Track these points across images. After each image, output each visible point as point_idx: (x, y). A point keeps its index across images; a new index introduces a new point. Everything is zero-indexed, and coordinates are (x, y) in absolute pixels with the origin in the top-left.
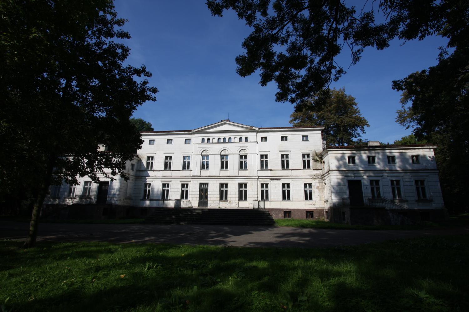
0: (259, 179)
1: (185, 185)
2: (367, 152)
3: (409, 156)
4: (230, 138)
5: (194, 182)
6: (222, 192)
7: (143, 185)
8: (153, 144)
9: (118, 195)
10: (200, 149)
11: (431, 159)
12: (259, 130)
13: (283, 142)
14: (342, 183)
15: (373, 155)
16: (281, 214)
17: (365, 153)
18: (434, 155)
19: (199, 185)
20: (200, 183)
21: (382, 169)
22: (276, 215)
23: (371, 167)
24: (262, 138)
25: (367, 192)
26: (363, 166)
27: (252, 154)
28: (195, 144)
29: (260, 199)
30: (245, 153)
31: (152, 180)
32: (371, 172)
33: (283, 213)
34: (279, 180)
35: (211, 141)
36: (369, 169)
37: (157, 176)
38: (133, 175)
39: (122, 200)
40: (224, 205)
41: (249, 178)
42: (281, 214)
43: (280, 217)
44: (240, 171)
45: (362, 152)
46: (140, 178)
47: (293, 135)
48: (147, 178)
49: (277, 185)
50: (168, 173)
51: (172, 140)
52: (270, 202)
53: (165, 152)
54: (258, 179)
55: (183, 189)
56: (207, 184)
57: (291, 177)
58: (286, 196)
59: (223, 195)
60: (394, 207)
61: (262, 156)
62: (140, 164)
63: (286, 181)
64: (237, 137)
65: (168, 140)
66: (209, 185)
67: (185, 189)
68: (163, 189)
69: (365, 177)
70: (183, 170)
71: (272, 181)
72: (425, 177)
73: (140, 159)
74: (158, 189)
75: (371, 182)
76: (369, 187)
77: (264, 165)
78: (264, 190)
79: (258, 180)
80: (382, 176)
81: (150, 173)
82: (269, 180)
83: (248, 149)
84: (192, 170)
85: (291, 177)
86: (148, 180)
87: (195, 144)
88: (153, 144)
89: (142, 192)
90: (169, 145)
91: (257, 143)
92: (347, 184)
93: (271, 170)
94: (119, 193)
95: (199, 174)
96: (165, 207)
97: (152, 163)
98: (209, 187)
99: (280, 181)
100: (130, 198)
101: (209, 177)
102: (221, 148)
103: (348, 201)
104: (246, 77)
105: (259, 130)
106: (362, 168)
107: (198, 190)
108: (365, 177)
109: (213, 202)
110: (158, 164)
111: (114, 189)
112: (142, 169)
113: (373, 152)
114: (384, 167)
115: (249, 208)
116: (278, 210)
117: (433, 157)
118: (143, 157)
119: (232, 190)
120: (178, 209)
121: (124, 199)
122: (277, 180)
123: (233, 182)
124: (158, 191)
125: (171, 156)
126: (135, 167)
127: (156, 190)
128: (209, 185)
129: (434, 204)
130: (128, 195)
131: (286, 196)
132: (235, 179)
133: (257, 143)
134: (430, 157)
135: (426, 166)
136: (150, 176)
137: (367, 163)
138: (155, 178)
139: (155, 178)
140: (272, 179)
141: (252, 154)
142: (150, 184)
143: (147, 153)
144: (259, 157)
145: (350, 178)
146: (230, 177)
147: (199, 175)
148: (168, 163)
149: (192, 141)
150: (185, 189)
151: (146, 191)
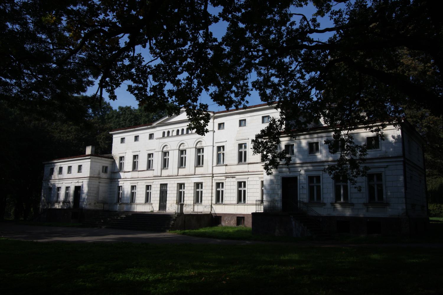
0: (215, 178)
1: (243, 183)
2: (307, 136)
3: (363, 138)
4: (169, 132)
5: (255, 179)
6: (239, 192)
7: (117, 187)
8: (245, 125)
9: (87, 199)
10: (161, 144)
11: (396, 140)
12: (215, 115)
13: (241, 128)
14: (275, 181)
15: (315, 140)
16: (233, 220)
17: (305, 139)
18: (401, 134)
19: (159, 186)
20: (161, 184)
21: (324, 159)
22: (229, 221)
23: (310, 159)
24: (241, 121)
25: (303, 195)
26: (301, 157)
27: (208, 146)
28: (157, 139)
29: (214, 202)
30: (202, 145)
31: (123, 182)
32: (308, 165)
33: (236, 219)
34: (235, 177)
35: (170, 135)
36: (308, 161)
37: (127, 177)
38: (106, 177)
39: (93, 204)
40: (200, 209)
41: (203, 176)
42: (233, 220)
43: (232, 224)
44: (197, 168)
45: (302, 137)
46: (114, 180)
47: (252, 117)
48: (119, 180)
49: (232, 183)
50: (135, 174)
51: (245, 120)
52: (224, 206)
53: (148, 149)
54: (213, 177)
55: (240, 189)
56: (167, 184)
57: (246, 174)
58: (241, 197)
59: (198, 198)
60: (335, 214)
61: (219, 148)
62: (115, 165)
63: (241, 178)
64: (174, 129)
65: (241, 121)
66: (168, 186)
67: (242, 189)
68: (132, 191)
69: (302, 172)
70: (147, 170)
71: (227, 179)
72: (383, 170)
73: (114, 160)
74: (128, 192)
75: (311, 179)
76: (306, 186)
77: (220, 159)
78: (241, 191)
79: (213, 178)
80: (385, 167)
81: (122, 174)
82: (224, 178)
83: (203, 140)
84: (154, 170)
85: (246, 174)
86: (120, 182)
87: (157, 139)
88: (245, 125)
89: (116, 196)
90: (242, 128)
91: (214, 132)
92: (280, 182)
93: (226, 165)
94: (87, 197)
95: (159, 174)
96: (138, 211)
97: (203, 156)
98: (168, 189)
99: (235, 178)
100: (104, 203)
101: (168, 176)
102: (179, 141)
103: (279, 205)
104: (293, 16)
105: (215, 115)
106: (300, 159)
107: (159, 192)
108: (302, 172)
109: (171, 205)
110: (128, 165)
111: (84, 194)
112: (116, 171)
113: (316, 136)
114: (327, 157)
115: (202, 212)
116: (231, 216)
117: (399, 136)
118: (117, 158)
119: (232, 191)
120: (181, 214)
121: (95, 203)
122: (232, 177)
123: (189, 181)
124: (127, 194)
125: (152, 153)
126: (109, 170)
127: (126, 193)
128: (168, 186)
129: (390, 210)
130: (101, 198)
131: (241, 197)
132: (191, 179)
133: (214, 132)
134: (393, 137)
135: (386, 152)
136: (122, 178)
137: (307, 153)
138: (126, 179)
139: (126, 179)
140: (227, 177)
141: (208, 146)
142: (122, 186)
143: (119, 153)
144: (215, 149)
145: (285, 175)
146: (186, 176)
147: (194, 172)
148: (222, 154)
149: (155, 136)
150: (242, 189)
151: (119, 193)
